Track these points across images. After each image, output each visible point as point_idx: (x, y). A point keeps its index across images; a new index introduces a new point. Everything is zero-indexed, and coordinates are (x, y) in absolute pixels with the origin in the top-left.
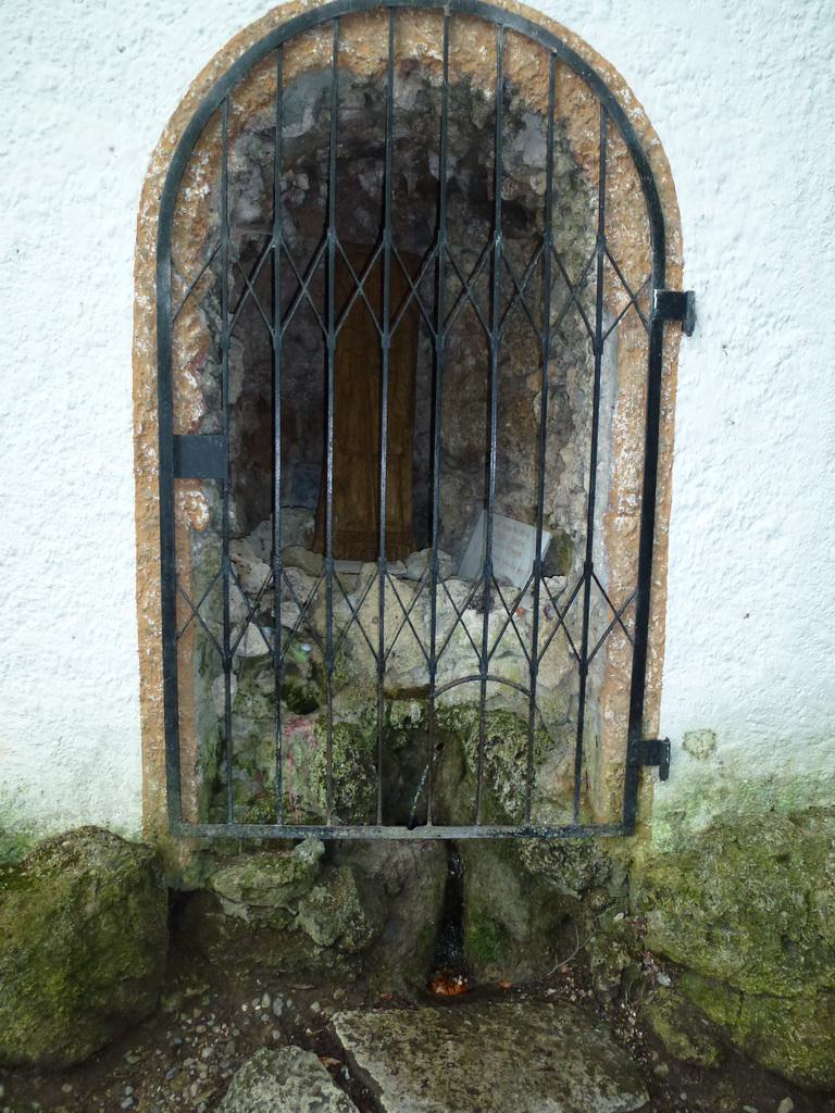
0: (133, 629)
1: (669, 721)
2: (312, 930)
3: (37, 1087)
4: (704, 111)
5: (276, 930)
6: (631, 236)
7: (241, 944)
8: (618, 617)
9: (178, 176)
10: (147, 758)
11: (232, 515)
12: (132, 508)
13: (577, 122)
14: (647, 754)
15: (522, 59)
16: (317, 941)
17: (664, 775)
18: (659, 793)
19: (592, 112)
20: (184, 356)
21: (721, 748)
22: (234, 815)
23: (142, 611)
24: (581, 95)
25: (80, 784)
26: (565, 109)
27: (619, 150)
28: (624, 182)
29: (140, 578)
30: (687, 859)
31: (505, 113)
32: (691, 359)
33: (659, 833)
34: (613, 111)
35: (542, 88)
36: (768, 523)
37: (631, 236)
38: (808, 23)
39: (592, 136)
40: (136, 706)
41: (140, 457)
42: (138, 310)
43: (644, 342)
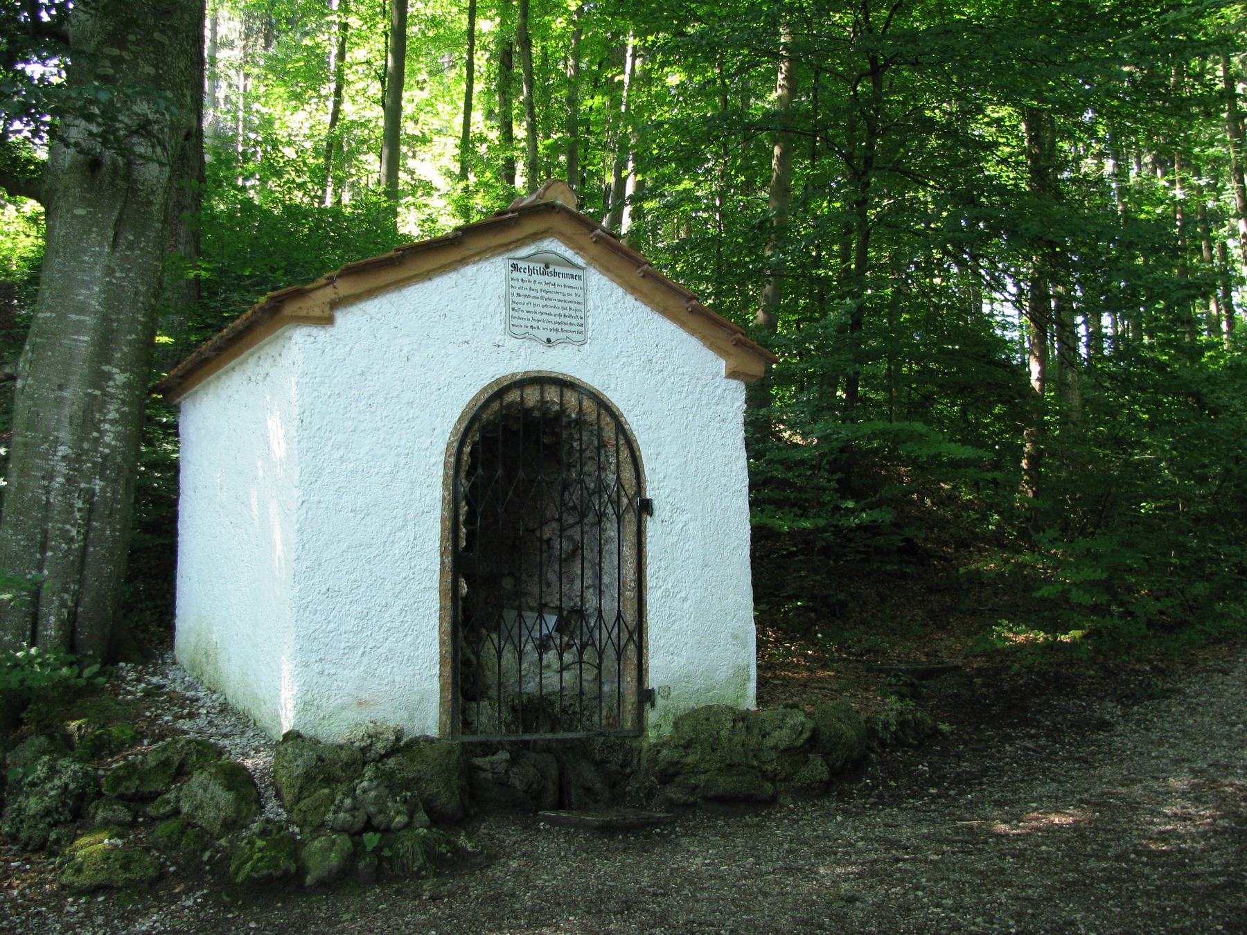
0: (437, 641)
1: (654, 680)
2: (518, 784)
3: (1240, 103)
4: (650, 427)
5: (502, 783)
6: (628, 475)
7: (1202, 151)
8: (631, 637)
9: (462, 444)
10: (442, 704)
11: (510, 215)
12: (437, 585)
13: (607, 428)
14: (646, 697)
15: (587, 404)
16: (1105, 576)
17: (653, 706)
18: (652, 716)
19: (612, 426)
20: (462, 518)
21: (673, 693)
22: (613, 151)
23: (441, 633)
24: (608, 419)
25: (411, 718)
26: (603, 424)
27: (622, 442)
28: (625, 453)
29: (440, 618)
30: (657, 748)
31: (580, 423)
32: (652, 527)
33: (652, 735)
34: (621, 428)
35: (594, 416)
36: (683, 594)
37: (628, 475)
38: (684, 395)
39: (613, 436)
40: (436, 679)
41: (442, 563)
42: (444, 498)
43: (634, 519)
